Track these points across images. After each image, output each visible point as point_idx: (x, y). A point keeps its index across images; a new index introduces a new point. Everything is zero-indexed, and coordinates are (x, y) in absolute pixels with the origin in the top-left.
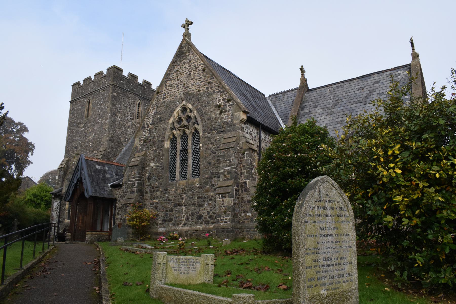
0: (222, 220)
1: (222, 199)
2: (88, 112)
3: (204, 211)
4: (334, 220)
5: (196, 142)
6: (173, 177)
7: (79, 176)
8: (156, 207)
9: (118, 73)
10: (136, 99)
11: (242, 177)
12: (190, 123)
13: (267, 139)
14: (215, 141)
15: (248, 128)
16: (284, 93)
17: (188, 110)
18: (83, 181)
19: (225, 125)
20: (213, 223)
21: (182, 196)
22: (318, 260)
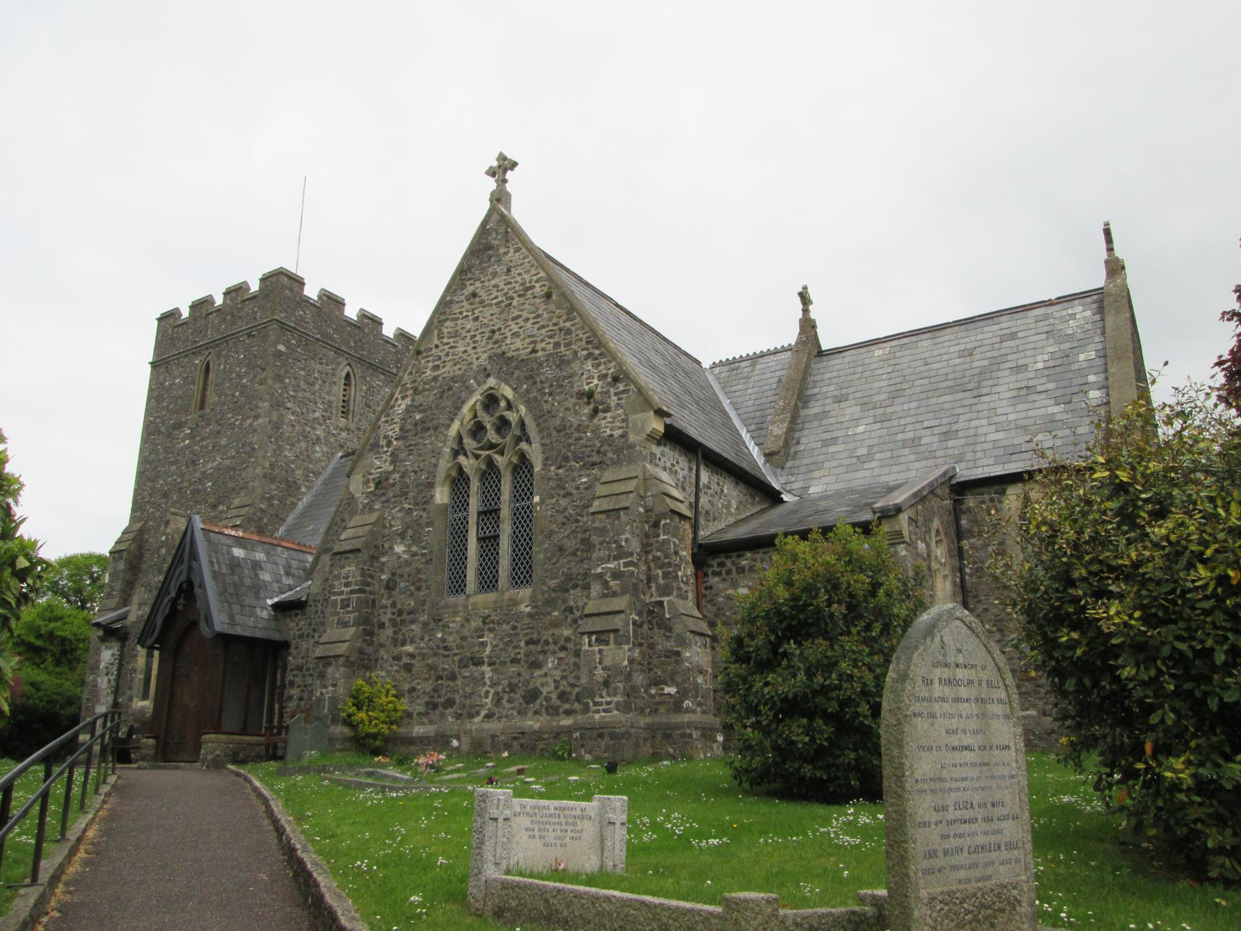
0: (596, 704)
1: (597, 649)
2: (204, 396)
3: (545, 680)
4: (975, 712)
5: (523, 490)
6: (458, 585)
7: (183, 578)
8: (408, 668)
9: (291, 289)
10: (338, 364)
11: (650, 588)
12: (508, 439)
13: (714, 486)
14: (577, 488)
15: (669, 455)
16: (754, 359)
17: (503, 404)
18: (197, 591)
19: (606, 447)
20: (569, 713)
21: (482, 636)
22: (944, 809)
